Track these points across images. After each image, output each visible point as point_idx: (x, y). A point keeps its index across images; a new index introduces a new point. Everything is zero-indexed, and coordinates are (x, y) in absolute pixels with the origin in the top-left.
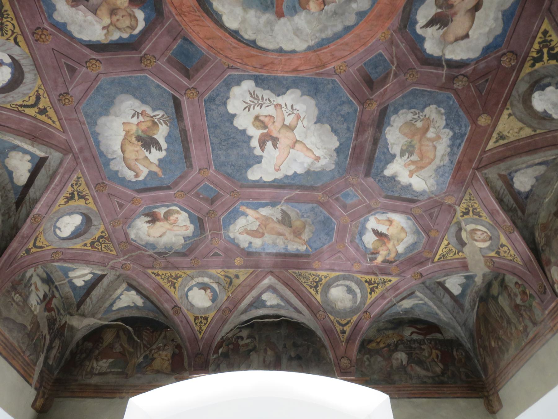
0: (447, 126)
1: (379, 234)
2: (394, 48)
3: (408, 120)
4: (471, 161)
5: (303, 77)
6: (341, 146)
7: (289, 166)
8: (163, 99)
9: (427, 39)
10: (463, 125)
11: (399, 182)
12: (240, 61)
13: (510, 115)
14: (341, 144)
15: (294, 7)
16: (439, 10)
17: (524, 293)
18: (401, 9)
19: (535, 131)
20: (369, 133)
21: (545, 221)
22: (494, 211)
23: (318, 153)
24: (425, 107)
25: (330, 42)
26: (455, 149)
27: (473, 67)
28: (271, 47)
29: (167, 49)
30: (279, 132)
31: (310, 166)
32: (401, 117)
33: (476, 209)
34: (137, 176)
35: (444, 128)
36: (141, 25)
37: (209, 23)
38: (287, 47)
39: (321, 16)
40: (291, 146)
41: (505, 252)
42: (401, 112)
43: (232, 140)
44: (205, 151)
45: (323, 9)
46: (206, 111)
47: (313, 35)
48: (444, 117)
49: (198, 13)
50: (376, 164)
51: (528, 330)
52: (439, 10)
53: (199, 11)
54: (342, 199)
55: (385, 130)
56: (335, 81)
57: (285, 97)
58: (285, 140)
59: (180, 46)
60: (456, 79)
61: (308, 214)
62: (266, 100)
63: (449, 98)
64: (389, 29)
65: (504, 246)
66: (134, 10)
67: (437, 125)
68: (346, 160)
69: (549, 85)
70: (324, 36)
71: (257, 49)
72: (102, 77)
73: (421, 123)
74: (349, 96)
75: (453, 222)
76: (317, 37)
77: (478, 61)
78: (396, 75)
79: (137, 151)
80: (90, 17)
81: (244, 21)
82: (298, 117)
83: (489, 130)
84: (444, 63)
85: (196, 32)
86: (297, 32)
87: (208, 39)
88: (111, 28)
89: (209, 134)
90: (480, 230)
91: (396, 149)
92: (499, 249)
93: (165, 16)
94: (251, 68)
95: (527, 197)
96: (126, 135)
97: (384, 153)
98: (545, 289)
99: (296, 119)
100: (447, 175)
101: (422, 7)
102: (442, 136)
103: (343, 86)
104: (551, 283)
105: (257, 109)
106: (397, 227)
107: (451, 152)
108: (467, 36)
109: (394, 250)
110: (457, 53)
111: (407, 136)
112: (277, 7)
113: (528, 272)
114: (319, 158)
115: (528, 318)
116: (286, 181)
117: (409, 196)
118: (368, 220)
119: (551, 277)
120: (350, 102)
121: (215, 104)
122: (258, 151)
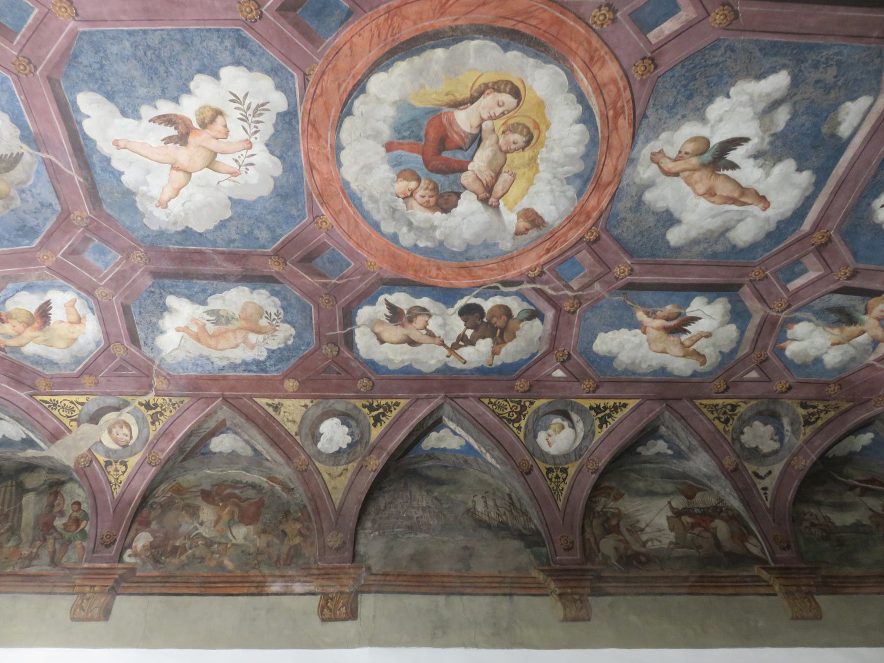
0: (271, 352)
1: (44, 313)
4: (232, 389)
7: (130, 163)
9: (374, 307)
12: (318, 92)
13: (306, 406)
14: (201, 234)
15: (400, 164)
16: (406, 312)
17: (77, 522)
18: (404, 277)
19: (297, 434)
20: (235, 268)
21: (185, 485)
22: (170, 435)
24: (289, 323)
26: (243, 367)
28: (344, 135)
30: (200, 146)
31: (144, 195)
32: (269, 300)
33: (162, 414)
35: (268, 349)
37: (375, 53)
38: (344, 156)
41: (116, 470)
44: (124, 18)
46: (218, 30)
47: (365, 188)
48: (282, 346)
49: (390, 39)
50: (182, 284)
51: (35, 562)
52: (406, 312)
53: (393, 40)
54: (91, 245)
56: (304, 218)
58: (182, 154)
61: (31, 200)
63: (309, 344)
64: (381, 268)
65: (126, 466)
67: (269, 341)
68: (174, 244)
69: (349, 426)
70: (365, 200)
74: (285, 236)
75: (124, 397)
77: (358, 358)
78: (325, 285)
81: (379, 101)
82: (234, 174)
83: (281, 394)
85: (361, 32)
86: (368, 169)
87: (351, 48)
89: (167, 30)
90: (130, 430)
91: (215, 302)
92: (116, 462)
95: (203, 454)
97: (204, 291)
98: (113, 543)
99: (231, 170)
100: (199, 369)
104: (126, 544)
105: (238, 114)
106: (73, 333)
107: (235, 365)
108: (382, 342)
109: (23, 341)
110: (363, 340)
112: (399, 144)
113: (111, 510)
114: (166, 207)
115: (51, 550)
116: (95, 159)
117: (141, 335)
118: (64, 291)
119: (133, 540)
120: (274, 239)
121: (234, 47)
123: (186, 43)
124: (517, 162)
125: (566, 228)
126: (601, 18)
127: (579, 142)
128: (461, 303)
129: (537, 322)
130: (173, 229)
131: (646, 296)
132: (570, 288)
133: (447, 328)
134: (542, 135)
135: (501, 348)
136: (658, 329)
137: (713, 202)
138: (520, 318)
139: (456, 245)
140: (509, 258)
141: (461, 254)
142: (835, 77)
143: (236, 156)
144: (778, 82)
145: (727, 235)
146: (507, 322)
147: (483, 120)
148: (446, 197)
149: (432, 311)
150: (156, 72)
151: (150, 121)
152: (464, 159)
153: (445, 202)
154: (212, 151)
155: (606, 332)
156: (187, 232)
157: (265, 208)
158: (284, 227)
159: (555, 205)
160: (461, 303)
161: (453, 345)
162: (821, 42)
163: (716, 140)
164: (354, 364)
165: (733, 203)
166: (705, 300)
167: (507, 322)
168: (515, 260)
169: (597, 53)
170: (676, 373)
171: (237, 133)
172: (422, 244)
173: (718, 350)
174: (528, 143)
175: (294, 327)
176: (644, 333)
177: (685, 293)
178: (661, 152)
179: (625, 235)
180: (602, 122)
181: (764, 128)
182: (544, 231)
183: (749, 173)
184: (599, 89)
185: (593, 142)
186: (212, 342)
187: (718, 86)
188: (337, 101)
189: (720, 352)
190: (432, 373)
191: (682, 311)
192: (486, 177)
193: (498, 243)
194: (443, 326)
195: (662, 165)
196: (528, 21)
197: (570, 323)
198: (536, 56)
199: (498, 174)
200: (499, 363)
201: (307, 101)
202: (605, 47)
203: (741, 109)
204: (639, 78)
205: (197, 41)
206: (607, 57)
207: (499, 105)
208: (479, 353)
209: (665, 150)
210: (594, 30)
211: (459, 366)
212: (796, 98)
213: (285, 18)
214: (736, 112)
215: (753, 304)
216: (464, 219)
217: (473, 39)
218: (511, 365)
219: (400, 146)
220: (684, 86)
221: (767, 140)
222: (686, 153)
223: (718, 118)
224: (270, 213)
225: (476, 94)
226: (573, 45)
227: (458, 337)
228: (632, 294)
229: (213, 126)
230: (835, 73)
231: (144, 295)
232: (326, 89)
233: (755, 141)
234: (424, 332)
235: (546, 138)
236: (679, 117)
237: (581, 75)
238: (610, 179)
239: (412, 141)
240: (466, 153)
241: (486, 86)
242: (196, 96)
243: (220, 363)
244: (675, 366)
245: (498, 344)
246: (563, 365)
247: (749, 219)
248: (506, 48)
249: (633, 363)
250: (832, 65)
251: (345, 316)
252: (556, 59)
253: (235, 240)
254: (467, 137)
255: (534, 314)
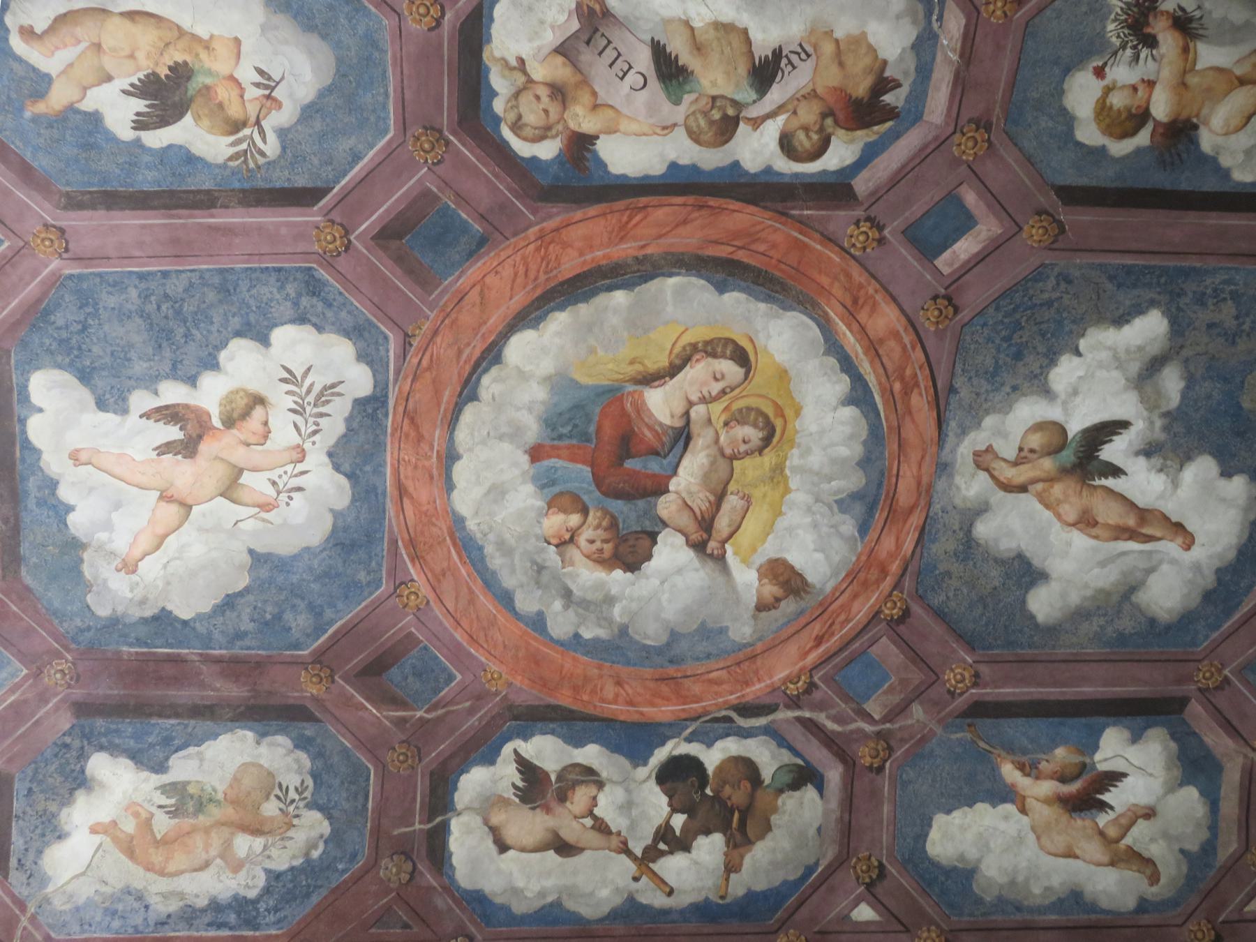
0: (274, 877)
2: (467, 704)
3: (279, 779)
5: (384, 511)
6: (179, 626)
7: (91, 490)
8: (316, 161)
9: (492, 768)
10: (281, 914)
11: (68, 800)
12: (425, 363)
14: (185, 623)
15: (553, 483)
16: (553, 778)
18: (553, 701)
20: (234, 691)
23: (151, 569)
24: (320, 808)
25: (474, 565)
26: (207, 918)
27: (435, 884)
29: (457, 194)
30: (217, 458)
31: (100, 547)
32: (289, 759)
34: (28, 33)
36: (522, 148)
37: (519, 300)
38: (461, 472)
39: (533, 540)
40: (169, 493)
42: (303, 756)
43: (182, 330)
44: (137, 254)
45: (549, 543)
46: (279, 270)
47: (491, 528)
49: (542, 277)
50: (127, 727)
52: (553, 778)
53: (547, 280)
55: (242, 728)
57: (328, 470)
58: (182, 473)
59: (465, 228)
60: (403, 857)
62: (317, 424)
63: (354, 857)
66: (559, 139)
67: (274, 852)
68: (131, 645)
70: (489, 550)
71: (457, 404)
72: (387, 22)
73: (278, 812)
76: (485, 535)
77: (450, 888)
78: (400, 723)
79: (132, 56)
80: (550, 39)
81: (522, 376)
82: (266, 507)
84: (439, 819)
85: (499, 269)
86: (498, 492)
88: (521, 79)
89: (201, 271)
91: (183, 767)
93: (539, 204)
94: (407, 388)
96: (195, 37)
99: (262, 500)
101: (560, 741)
102: (243, 873)
103: (366, 607)
105: (289, 402)
108: (503, 847)
110: (465, 842)
111: (231, 786)
112: (553, 447)
116: (32, 484)
120: (319, 630)
121: (299, 295)
122: (141, 401)
123: (226, 290)
124: (751, 474)
125: (846, 594)
126: (862, 238)
127: (852, 437)
128: (661, 755)
129: (810, 792)
130: (136, 613)
131: (1014, 728)
132: (867, 717)
133: (634, 812)
134: (790, 426)
135: (742, 857)
136: (1047, 801)
137: (1096, 537)
138: (778, 785)
139: (651, 633)
140: (748, 658)
141: (659, 651)
142: (1237, 318)
143: (274, 475)
144: (1149, 328)
145: (1134, 598)
146: (752, 797)
147: (691, 404)
148: (631, 542)
149: (604, 774)
150: (169, 334)
151: (141, 417)
152: (662, 472)
153: (629, 551)
154: (235, 466)
155: (949, 812)
156: (163, 620)
157: (311, 569)
158: (340, 605)
159: (822, 550)
160: (661, 755)
161: (646, 850)
162: (1198, 265)
163: (1075, 427)
164: (441, 902)
165: (1130, 538)
166: (1126, 734)
167: (752, 797)
168: (759, 661)
169: (862, 292)
170: (1104, 903)
171: (283, 432)
172: (587, 634)
173: (1177, 847)
174: (767, 440)
175: (329, 817)
176: (1023, 811)
177: (1083, 720)
178: (989, 450)
179: (953, 604)
180: (885, 403)
181: (1150, 402)
182: (809, 602)
183: (1143, 483)
184: (873, 348)
185: (875, 436)
186: (157, 857)
187: (1058, 339)
188: (455, 378)
189: (1182, 851)
190: (601, 920)
191: (1088, 760)
192: (701, 502)
193: (727, 628)
194: (627, 806)
195: (996, 473)
196: (753, 247)
197: (874, 795)
198: (768, 299)
199: (720, 497)
200: (741, 892)
201: (405, 378)
202: (873, 281)
203: (1102, 374)
204: (932, 329)
205: (244, 285)
206: (878, 297)
207: (716, 379)
208: (695, 870)
209: (995, 446)
210: (853, 257)
211: (658, 900)
212: (1186, 353)
213: (385, 249)
214: (1098, 377)
215: (1217, 741)
216: (662, 583)
217: (671, 275)
218: (765, 895)
219: (554, 452)
220: (1007, 339)
221: (1159, 423)
222: (1032, 451)
223: (1070, 390)
224: (318, 579)
225: (677, 362)
226: (825, 281)
227: (657, 832)
228: (985, 724)
229: (245, 424)
230: (1233, 311)
231: (48, 754)
232: (438, 358)
233: (1139, 426)
234: (588, 822)
235: (797, 432)
236: (1007, 389)
237: (842, 327)
238: (912, 501)
239: (574, 442)
240: (665, 462)
241: (694, 347)
242: (226, 373)
243: (161, 908)
244: (1100, 887)
245: (736, 846)
246: (871, 892)
247: (1165, 567)
248: (721, 288)
249: (1013, 883)
250: (1225, 299)
251: (433, 790)
252: (800, 303)
253: (246, 634)
254: (665, 433)
255: (804, 776)
